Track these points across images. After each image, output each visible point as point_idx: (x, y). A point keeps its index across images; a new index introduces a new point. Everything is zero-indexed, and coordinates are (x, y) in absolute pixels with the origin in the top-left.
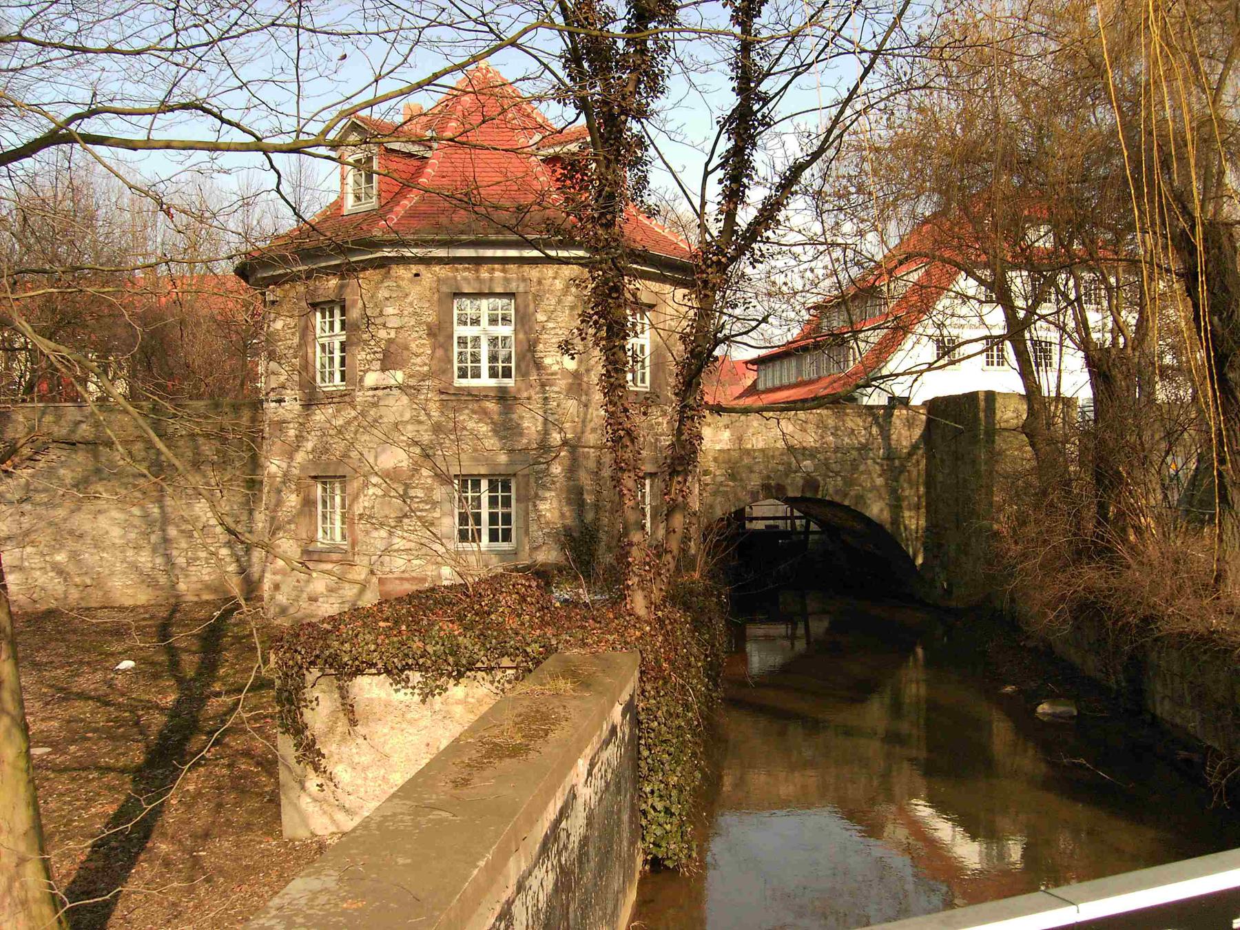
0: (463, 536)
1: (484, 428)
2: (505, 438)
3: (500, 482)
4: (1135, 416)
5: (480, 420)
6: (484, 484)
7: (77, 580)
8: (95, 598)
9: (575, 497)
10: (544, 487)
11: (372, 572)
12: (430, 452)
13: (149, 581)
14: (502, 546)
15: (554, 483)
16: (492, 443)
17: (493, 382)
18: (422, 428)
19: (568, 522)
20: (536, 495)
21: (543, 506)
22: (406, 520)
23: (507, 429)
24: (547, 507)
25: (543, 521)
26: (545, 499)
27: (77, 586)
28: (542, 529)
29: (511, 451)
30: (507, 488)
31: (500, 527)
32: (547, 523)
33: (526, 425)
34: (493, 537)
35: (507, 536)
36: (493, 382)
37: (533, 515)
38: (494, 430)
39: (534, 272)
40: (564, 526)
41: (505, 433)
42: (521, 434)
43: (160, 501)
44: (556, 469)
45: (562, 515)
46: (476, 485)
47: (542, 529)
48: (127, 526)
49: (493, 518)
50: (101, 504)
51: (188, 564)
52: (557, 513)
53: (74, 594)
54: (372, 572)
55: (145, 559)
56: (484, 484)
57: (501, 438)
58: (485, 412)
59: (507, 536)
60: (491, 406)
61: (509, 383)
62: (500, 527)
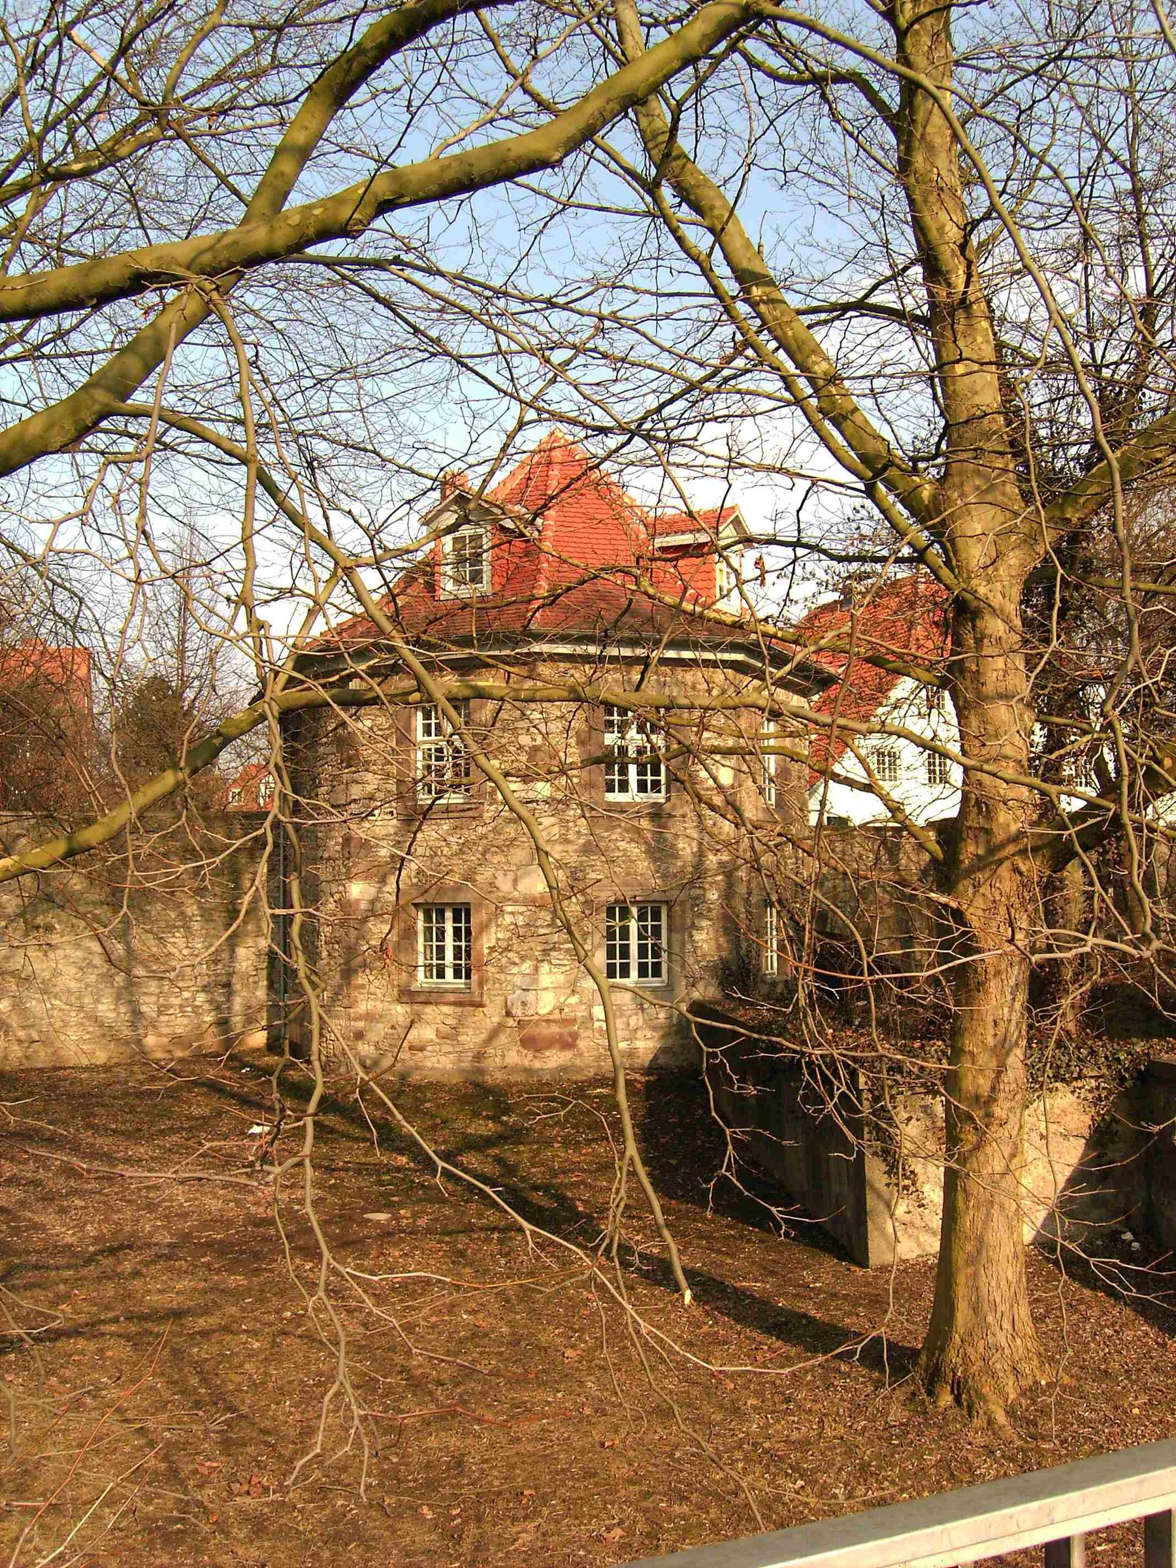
0: (611, 973)
1: (635, 850)
2: (660, 859)
3: (650, 910)
4: (282, 863)
5: (632, 840)
6: (449, 915)
7: (21, 1034)
8: (42, 1058)
9: (729, 926)
10: (700, 915)
11: (508, 1014)
12: (580, 875)
13: (108, 1034)
14: (654, 982)
15: (709, 910)
16: (644, 865)
17: (640, 798)
18: (570, 848)
19: (724, 954)
20: (693, 926)
21: (699, 936)
22: (553, 954)
23: (660, 851)
24: (704, 936)
25: (699, 952)
26: (701, 928)
27: (20, 1041)
28: (698, 962)
29: (664, 877)
30: (656, 916)
31: (650, 960)
32: (704, 956)
33: (681, 846)
34: (643, 972)
35: (657, 972)
36: (640, 798)
37: (689, 946)
38: (647, 852)
39: (689, 676)
40: (721, 959)
41: (657, 855)
42: (676, 857)
43: (123, 935)
44: (713, 895)
45: (719, 947)
46: (625, 914)
47: (698, 962)
48: (84, 967)
49: (457, 949)
50: (55, 939)
51: (160, 1013)
52: (713, 944)
53: (16, 1051)
54: (508, 1014)
55: (106, 1009)
56: (449, 915)
57: (655, 861)
58: (638, 831)
59: (657, 972)
60: (645, 824)
61: (660, 797)
62: (650, 960)
